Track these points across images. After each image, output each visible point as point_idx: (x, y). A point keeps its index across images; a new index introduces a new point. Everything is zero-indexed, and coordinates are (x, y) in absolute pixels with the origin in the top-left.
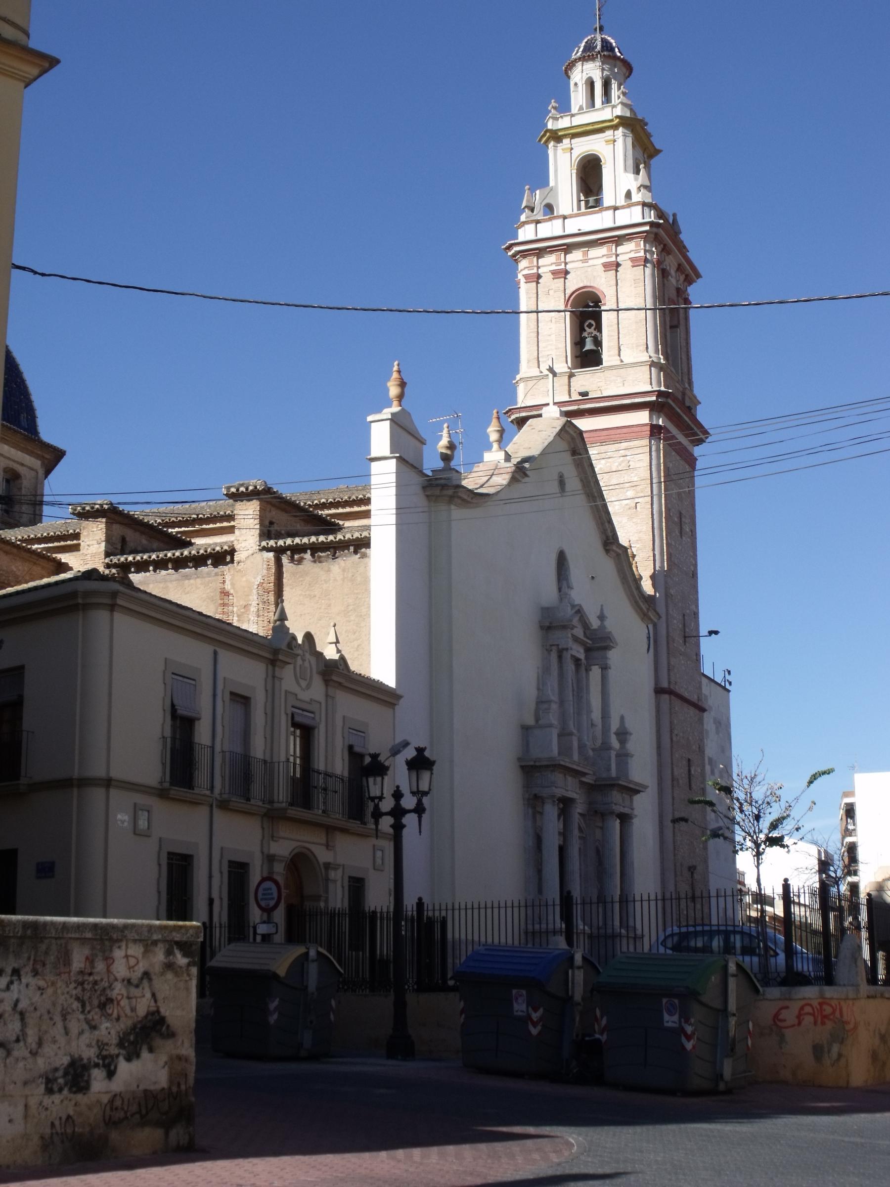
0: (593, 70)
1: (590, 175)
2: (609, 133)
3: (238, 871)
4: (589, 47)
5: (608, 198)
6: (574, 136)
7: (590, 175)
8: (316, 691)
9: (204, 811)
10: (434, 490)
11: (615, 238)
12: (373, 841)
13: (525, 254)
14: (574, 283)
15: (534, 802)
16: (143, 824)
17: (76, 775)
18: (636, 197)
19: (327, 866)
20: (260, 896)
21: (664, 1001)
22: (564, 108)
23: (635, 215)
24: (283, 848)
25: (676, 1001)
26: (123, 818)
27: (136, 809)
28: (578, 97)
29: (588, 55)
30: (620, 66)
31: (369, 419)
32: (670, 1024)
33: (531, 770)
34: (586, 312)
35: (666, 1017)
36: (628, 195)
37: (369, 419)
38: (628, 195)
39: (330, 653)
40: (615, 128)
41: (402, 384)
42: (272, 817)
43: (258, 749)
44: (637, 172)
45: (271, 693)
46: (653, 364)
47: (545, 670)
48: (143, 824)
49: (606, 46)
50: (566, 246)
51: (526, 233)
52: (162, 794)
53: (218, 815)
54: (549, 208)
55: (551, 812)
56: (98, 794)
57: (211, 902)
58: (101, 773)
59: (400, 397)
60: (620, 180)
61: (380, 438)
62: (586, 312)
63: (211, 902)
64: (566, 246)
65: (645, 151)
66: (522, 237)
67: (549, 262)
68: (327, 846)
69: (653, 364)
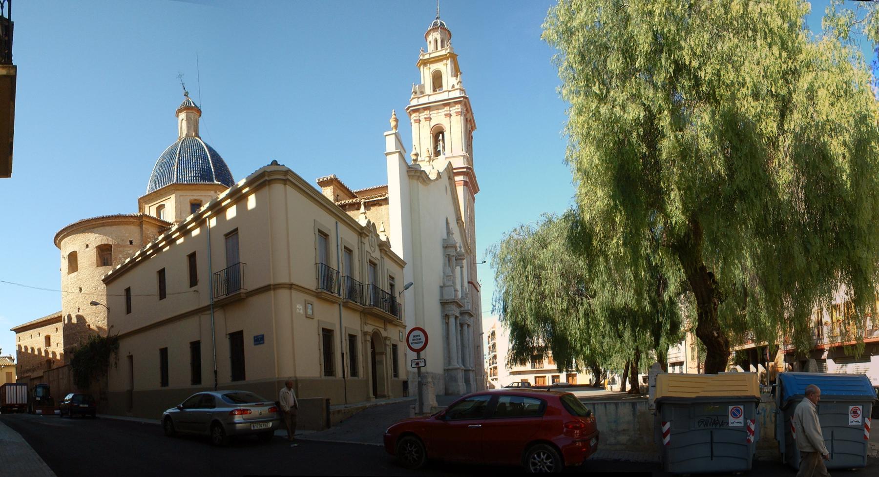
0: (437, 35)
1: (437, 80)
2: (445, 61)
3: (352, 338)
4: (436, 24)
5: (445, 88)
6: (431, 63)
7: (437, 80)
8: (376, 254)
9: (337, 306)
10: (413, 173)
11: (447, 104)
12: (400, 328)
13: (415, 111)
14: (433, 123)
15: (446, 317)
16: (309, 312)
17: (272, 282)
18: (457, 87)
19: (386, 338)
20: (411, 341)
21: (731, 408)
22: (425, 50)
23: (457, 94)
24: (369, 329)
25: (742, 407)
26: (299, 308)
27: (306, 303)
28: (431, 48)
29: (435, 29)
30: (447, 34)
31: (385, 134)
32: (736, 425)
33: (444, 304)
34: (438, 134)
35: (731, 419)
36: (453, 86)
37: (385, 134)
38: (453, 86)
39: (383, 238)
40: (447, 59)
41: (397, 120)
42: (366, 314)
43: (357, 277)
44: (457, 76)
45: (361, 249)
46: (464, 156)
47: (445, 265)
48: (309, 312)
49: (442, 24)
50: (428, 108)
51: (414, 102)
52: (318, 295)
53: (343, 310)
54: (422, 93)
55: (452, 320)
56: (284, 293)
57: (343, 354)
58: (285, 280)
59: (396, 127)
60: (449, 80)
61: (391, 144)
62: (438, 134)
63: (343, 354)
64: (428, 108)
65: (456, 71)
66: (412, 103)
67: (423, 115)
68: (385, 329)
69: (464, 156)
